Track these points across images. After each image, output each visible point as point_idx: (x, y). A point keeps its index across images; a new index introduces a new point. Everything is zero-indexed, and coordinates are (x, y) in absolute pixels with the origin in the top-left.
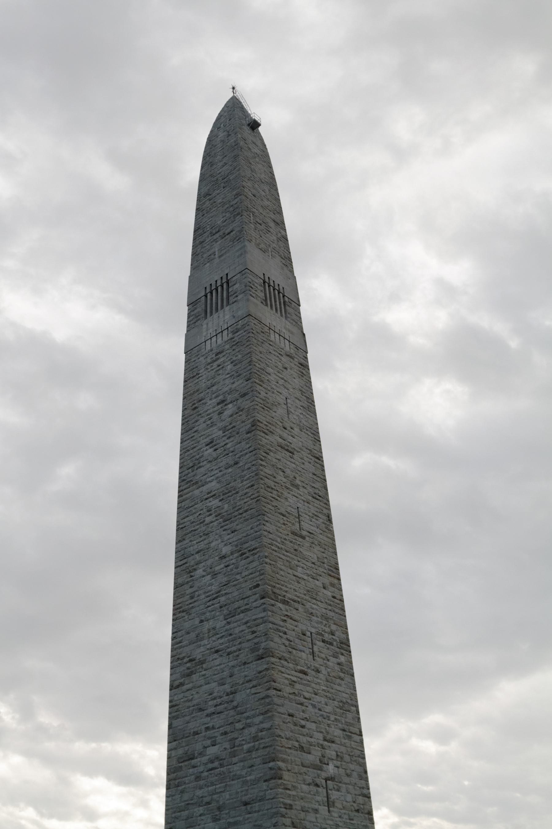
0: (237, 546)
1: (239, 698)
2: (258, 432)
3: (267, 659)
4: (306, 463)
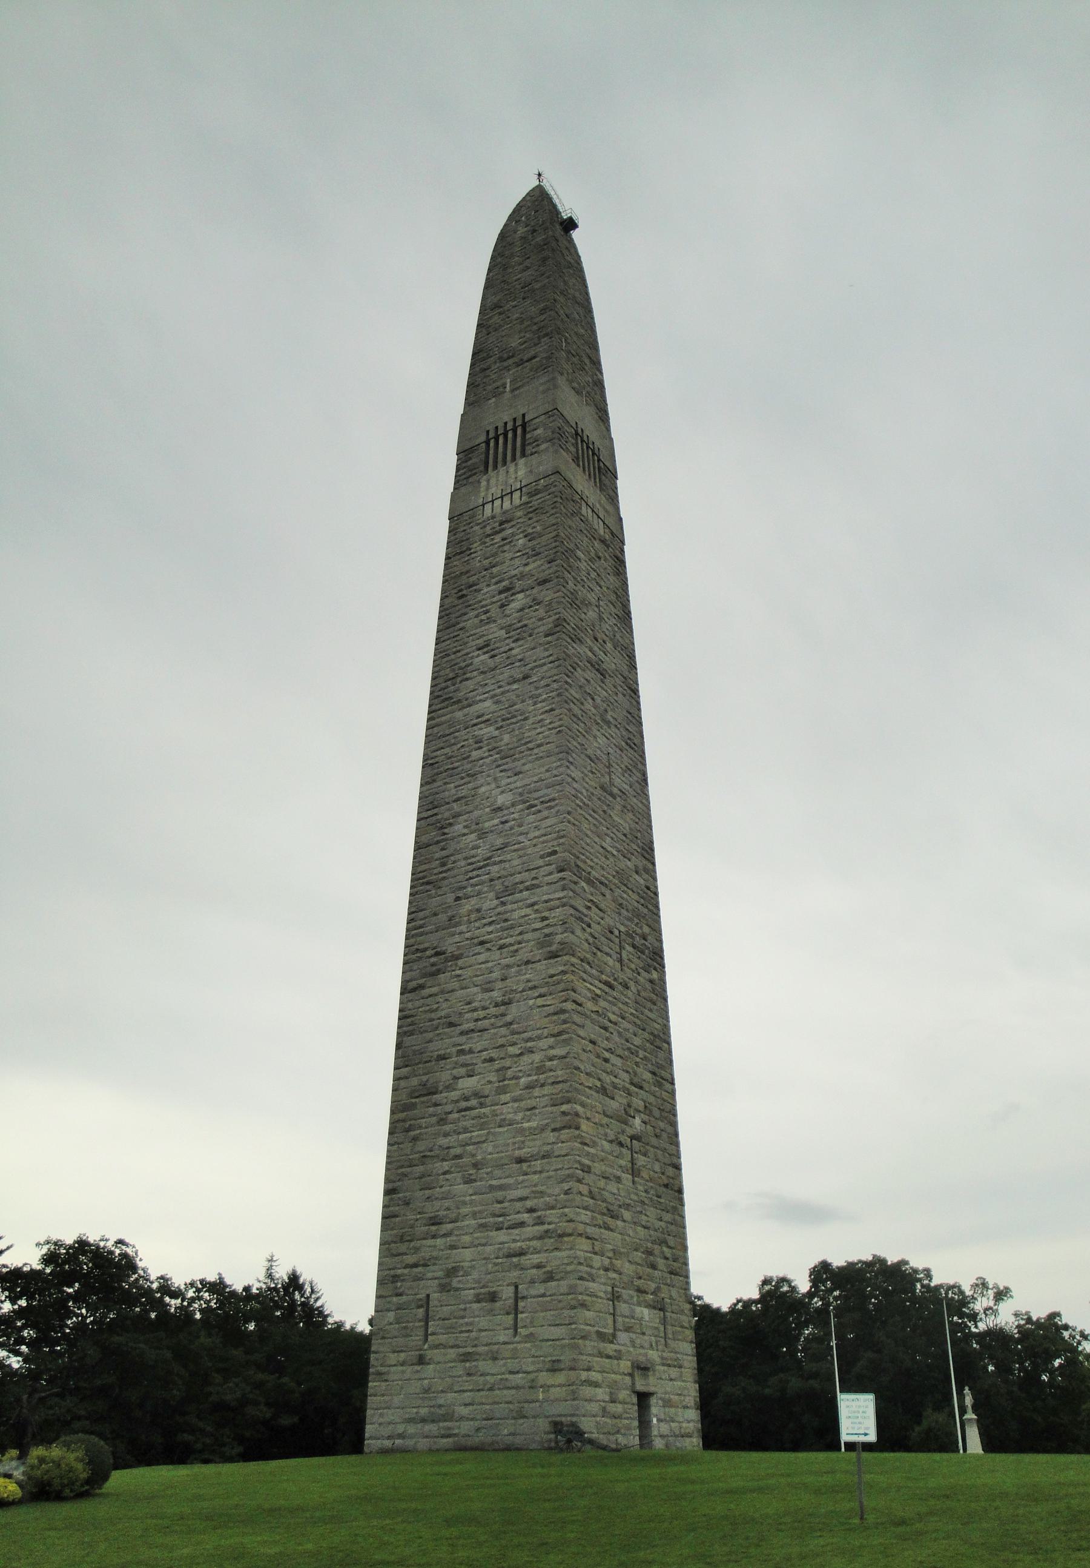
0: (521, 794)
1: (513, 1011)
2: (564, 636)
3: (566, 958)
4: (620, 695)
